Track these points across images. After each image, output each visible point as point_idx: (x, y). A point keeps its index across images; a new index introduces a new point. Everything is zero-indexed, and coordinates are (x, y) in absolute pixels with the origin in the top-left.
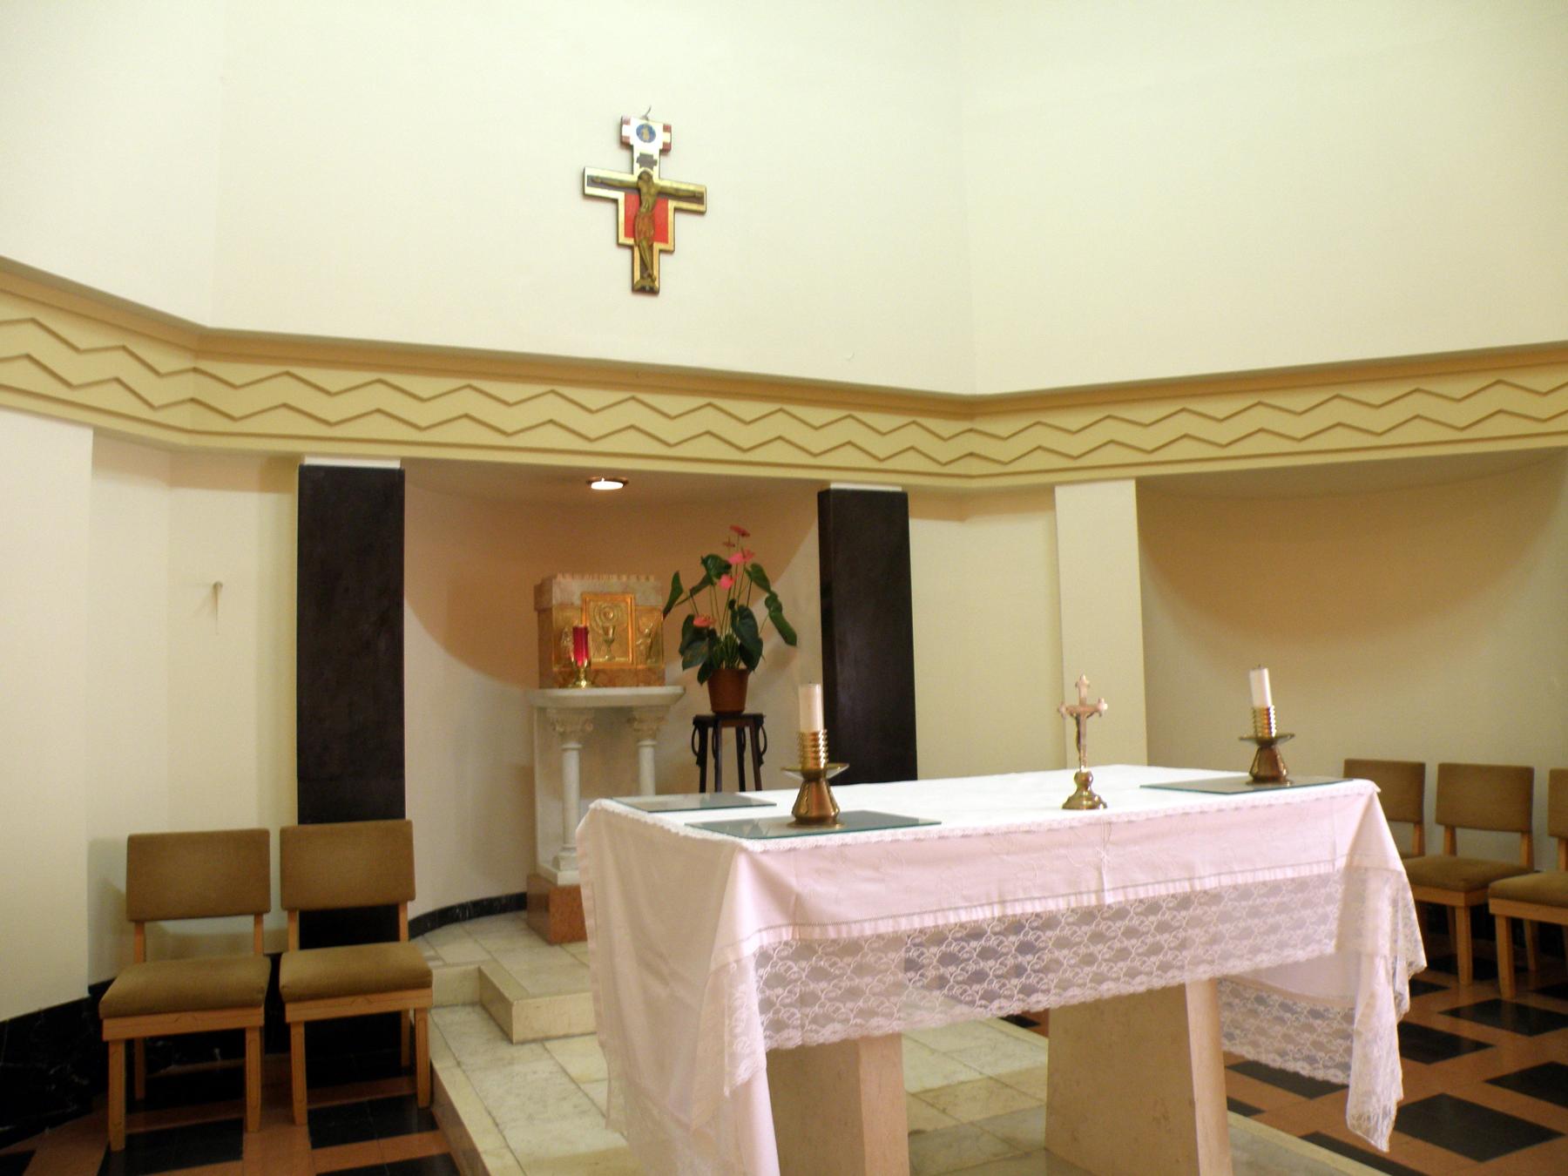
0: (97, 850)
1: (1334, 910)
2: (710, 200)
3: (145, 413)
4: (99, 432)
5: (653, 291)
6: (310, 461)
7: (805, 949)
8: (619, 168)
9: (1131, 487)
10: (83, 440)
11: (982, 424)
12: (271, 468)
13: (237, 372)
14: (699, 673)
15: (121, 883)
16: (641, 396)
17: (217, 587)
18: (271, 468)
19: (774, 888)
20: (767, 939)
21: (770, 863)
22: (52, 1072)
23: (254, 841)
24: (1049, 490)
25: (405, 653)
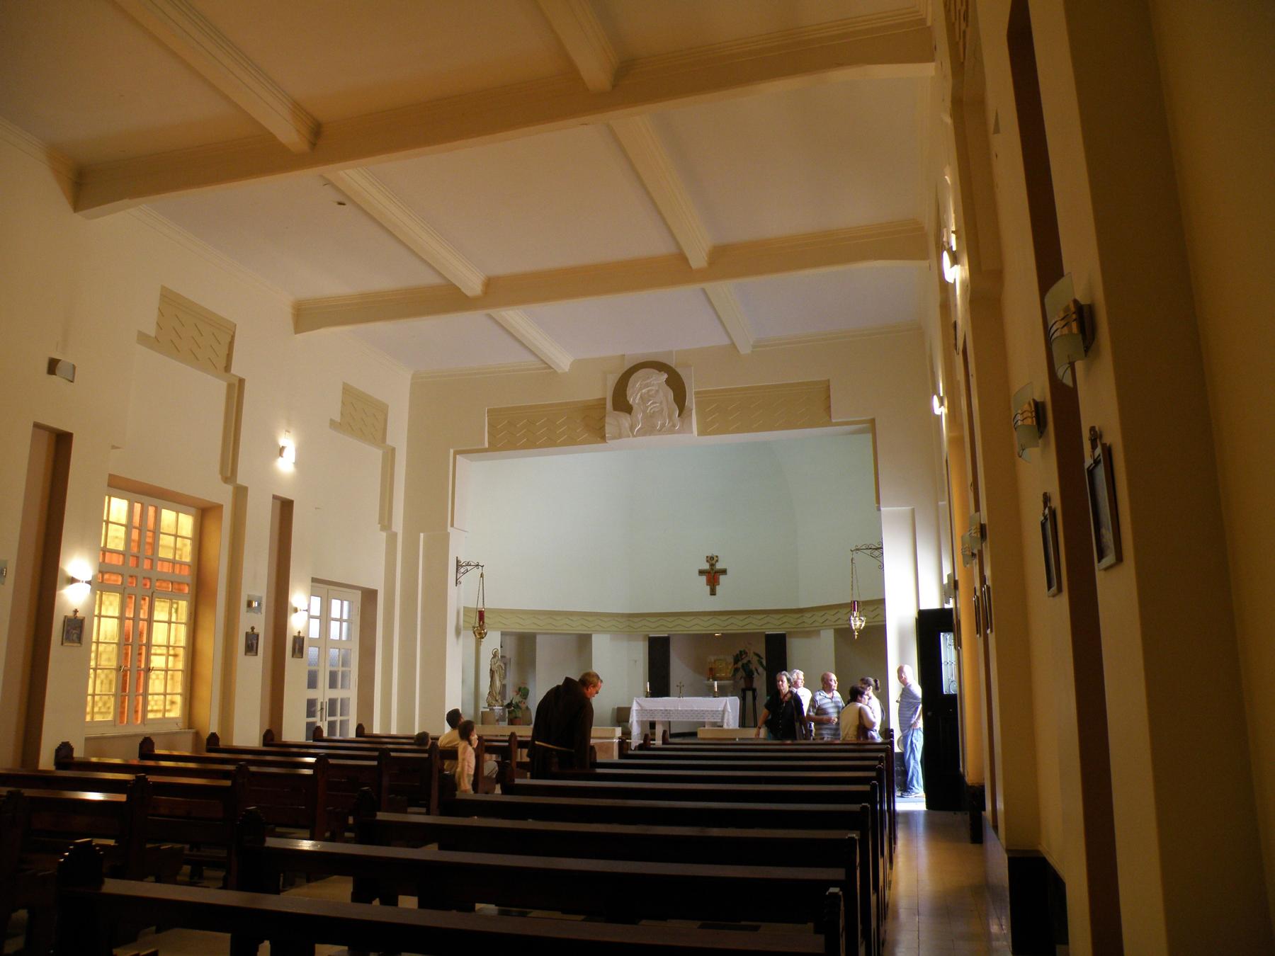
0: (613, 709)
1: (720, 716)
3: (572, 629)
5: (715, 594)
6: (767, 633)
7: (642, 710)
8: (706, 566)
9: (833, 630)
16: (665, 618)
20: (637, 708)
22: (148, 846)
24: (819, 631)
25: (286, 673)
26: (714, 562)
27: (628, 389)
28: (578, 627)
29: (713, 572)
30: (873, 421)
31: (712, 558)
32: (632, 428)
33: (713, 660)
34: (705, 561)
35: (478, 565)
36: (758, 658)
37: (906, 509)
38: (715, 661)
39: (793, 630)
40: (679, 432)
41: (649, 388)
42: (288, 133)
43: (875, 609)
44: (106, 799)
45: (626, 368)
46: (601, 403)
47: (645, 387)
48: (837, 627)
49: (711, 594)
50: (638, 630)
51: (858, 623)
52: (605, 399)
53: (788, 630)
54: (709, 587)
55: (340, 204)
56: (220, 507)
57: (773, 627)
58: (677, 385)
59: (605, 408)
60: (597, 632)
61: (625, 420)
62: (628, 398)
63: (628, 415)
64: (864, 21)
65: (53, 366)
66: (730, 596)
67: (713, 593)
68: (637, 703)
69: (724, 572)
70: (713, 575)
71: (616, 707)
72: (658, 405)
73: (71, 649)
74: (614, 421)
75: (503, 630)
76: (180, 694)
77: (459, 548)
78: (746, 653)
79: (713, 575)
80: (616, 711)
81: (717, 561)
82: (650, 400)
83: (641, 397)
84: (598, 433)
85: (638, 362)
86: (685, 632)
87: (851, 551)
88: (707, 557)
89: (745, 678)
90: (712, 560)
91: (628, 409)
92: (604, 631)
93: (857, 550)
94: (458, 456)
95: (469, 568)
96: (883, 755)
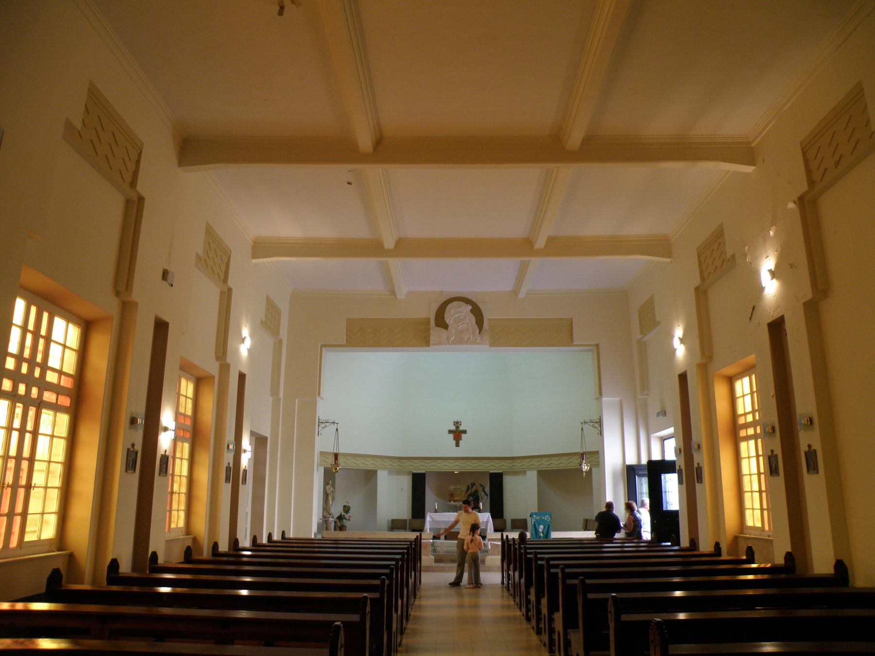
0: (388, 521)
2: (467, 432)
3: (393, 468)
4: (388, 471)
5: (458, 446)
6: (414, 472)
8: (453, 428)
9: (536, 471)
10: (387, 472)
11: (483, 461)
12: (409, 473)
13: (358, 459)
14: (847, 568)
15: (390, 525)
16: (424, 461)
17: (402, 489)
18: (409, 473)
19: (431, 517)
21: (433, 516)
23: (405, 521)
26: (458, 425)
27: (445, 313)
28: (369, 465)
29: (458, 432)
30: (597, 346)
31: (457, 423)
32: (448, 339)
33: (453, 489)
34: (453, 424)
35: (334, 423)
36: (482, 488)
37: (617, 399)
38: (454, 489)
39: (518, 470)
40: (479, 344)
41: (460, 314)
42: (365, 141)
43: (590, 458)
44: (715, 577)
45: (444, 300)
46: (427, 321)
47: (457, 314)
48: (539, 469)
49: (456, 446)
50: (417, 468)
51: (586, 467)
52: (429, 319)
53: (503, 470)
54: (455, 441)
55: (349, 183)
56: (213, 377)
57: (494, 468)
58: (477, 312)
59: (429, 324)
60: (381, 469)
61: (443, 333)
62: (446, 319)
63: (445, 331)
64: (741, 138)
65: (165, 275)
66: (469, 447)
67: (457, 445)
68: (430, 516)
69: (465, 432)
70: (457, 433)
71: (391, 519)
72: (465, 325)
73: (163, 478)
74: (436, 333)
75: (325, 466)
76: (183, 510)
77: (323, 410)
78: (475, 484)
79: (457, 434)
80: (390, 523)
81: (461, 425)
82: (460, 322)
83: (454, 319)
84: (425, 341)
85: (453, 296)
86: (437, 470)
87: (582, 423)
88: (454, 422)
89: (474, 501)
90: (457, 424)
91: (445, 326)
92: (384, 468)
93: (585, 422)
94: (323, 348)
95: (327, 424)
96: (405, 551)
